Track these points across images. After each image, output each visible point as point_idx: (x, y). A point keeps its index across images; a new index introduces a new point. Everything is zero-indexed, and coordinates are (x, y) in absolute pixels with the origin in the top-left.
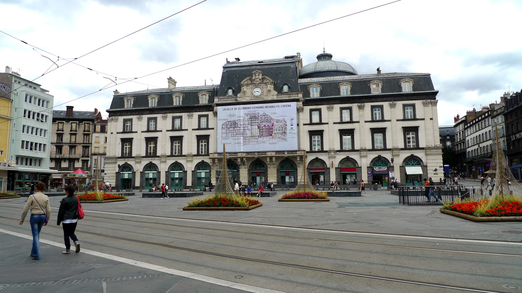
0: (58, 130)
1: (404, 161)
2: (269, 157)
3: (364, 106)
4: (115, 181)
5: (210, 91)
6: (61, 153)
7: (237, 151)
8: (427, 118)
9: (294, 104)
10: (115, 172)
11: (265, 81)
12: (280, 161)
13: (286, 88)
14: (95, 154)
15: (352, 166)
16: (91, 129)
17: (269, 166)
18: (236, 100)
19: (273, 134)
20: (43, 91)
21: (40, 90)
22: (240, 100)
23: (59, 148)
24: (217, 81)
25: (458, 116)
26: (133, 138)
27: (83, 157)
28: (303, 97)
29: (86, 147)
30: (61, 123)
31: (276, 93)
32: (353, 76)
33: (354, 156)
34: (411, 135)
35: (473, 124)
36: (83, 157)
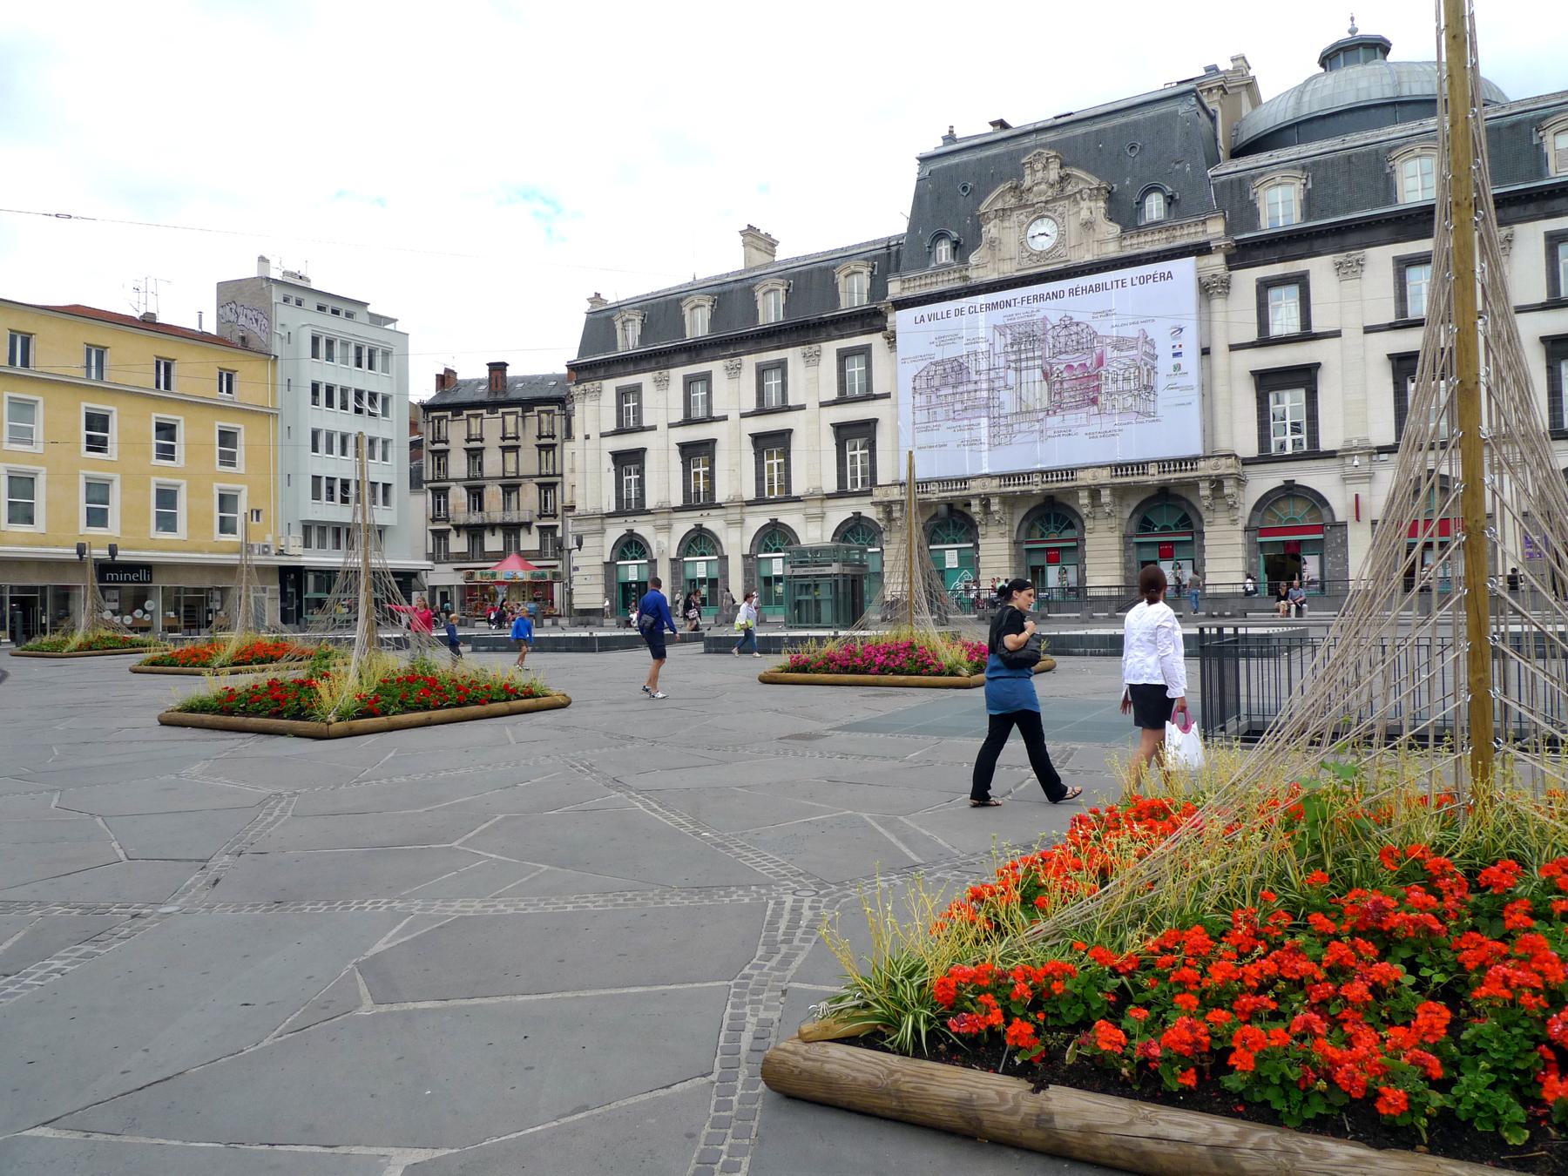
0: (468, 440)
2: (1088, 487)
7: (968, 473)
9: (1185, 269)
10: (599, 561)
11: (1070, 189)
12: (1134, 504)
13: (1155, 207)
18: (966, 278)
19: (1102, 399)
20: (379, 320)
21: (366, 320)
22: (978, 276)
24: (890, 216)
27: (540, 516)
28: (1229, 230)
30: (476, 416)
31: (1116, 229)
34: (1290, 402)
36: (540, 516)
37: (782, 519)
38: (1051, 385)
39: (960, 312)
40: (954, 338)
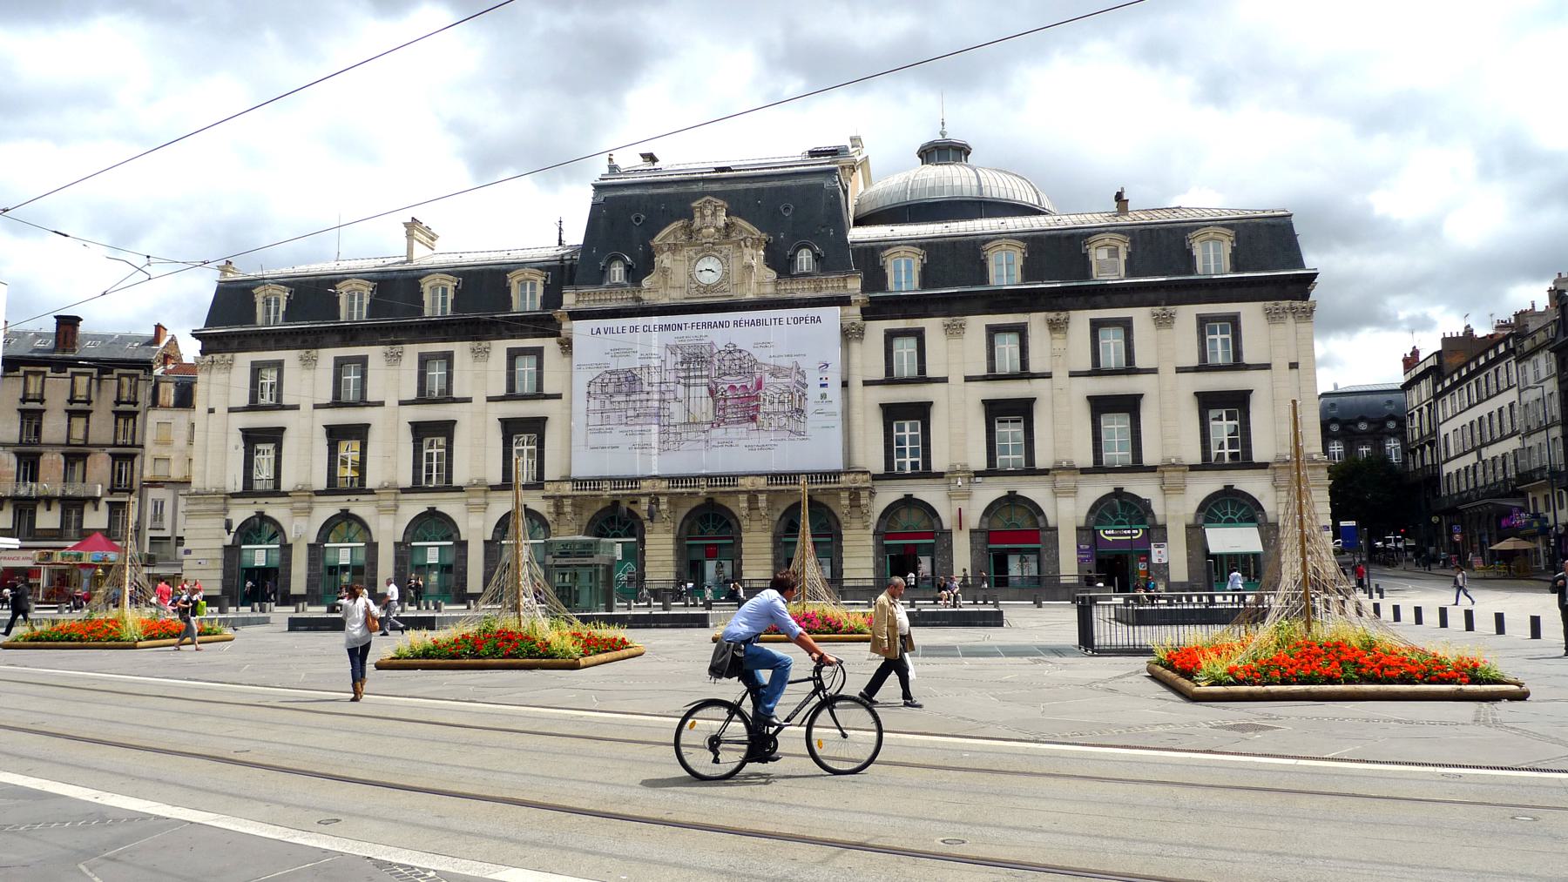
1: (1201, 508)
2: (748, 492)
3: (1171, 316)
4: (219, 575)
5: (548, 269)
6: (34, 479)
7: (638, 473)
8: (1280, 364)
9: (832, 315)
10: (219, 544)
13: (805, 259)
14: (154, 484)
15: (1026, 524)
16: (144, 395)
17: (745, 523)
18: (639, 299)
19: (760, 417)
22: (649, 298)
23: (29, 464)
25: (1415, 353)
26: (368, 426)
29: (124, 457)
30: (36, 374)
32: (1041, 218)
33: (1032, 490)
34: (524, 446)
35: (1462, 380)
36: (112, 491)
37: (1021, 492)
38: (716, 401)
39: (634, 329)
40: (627, 352)
